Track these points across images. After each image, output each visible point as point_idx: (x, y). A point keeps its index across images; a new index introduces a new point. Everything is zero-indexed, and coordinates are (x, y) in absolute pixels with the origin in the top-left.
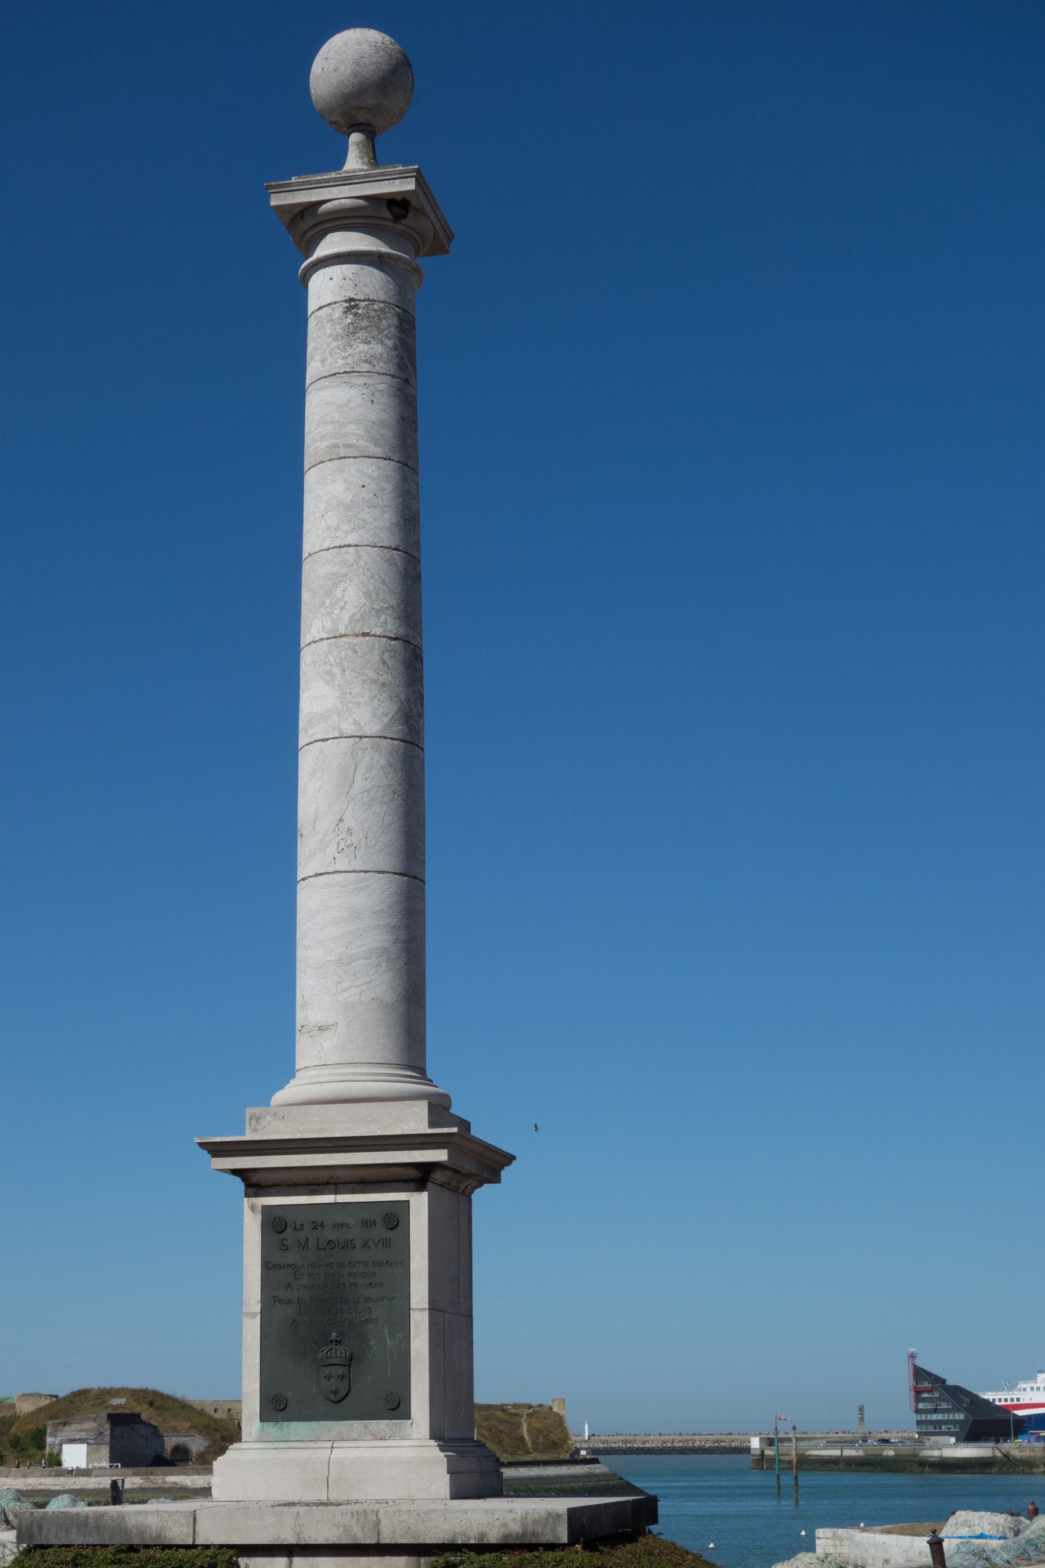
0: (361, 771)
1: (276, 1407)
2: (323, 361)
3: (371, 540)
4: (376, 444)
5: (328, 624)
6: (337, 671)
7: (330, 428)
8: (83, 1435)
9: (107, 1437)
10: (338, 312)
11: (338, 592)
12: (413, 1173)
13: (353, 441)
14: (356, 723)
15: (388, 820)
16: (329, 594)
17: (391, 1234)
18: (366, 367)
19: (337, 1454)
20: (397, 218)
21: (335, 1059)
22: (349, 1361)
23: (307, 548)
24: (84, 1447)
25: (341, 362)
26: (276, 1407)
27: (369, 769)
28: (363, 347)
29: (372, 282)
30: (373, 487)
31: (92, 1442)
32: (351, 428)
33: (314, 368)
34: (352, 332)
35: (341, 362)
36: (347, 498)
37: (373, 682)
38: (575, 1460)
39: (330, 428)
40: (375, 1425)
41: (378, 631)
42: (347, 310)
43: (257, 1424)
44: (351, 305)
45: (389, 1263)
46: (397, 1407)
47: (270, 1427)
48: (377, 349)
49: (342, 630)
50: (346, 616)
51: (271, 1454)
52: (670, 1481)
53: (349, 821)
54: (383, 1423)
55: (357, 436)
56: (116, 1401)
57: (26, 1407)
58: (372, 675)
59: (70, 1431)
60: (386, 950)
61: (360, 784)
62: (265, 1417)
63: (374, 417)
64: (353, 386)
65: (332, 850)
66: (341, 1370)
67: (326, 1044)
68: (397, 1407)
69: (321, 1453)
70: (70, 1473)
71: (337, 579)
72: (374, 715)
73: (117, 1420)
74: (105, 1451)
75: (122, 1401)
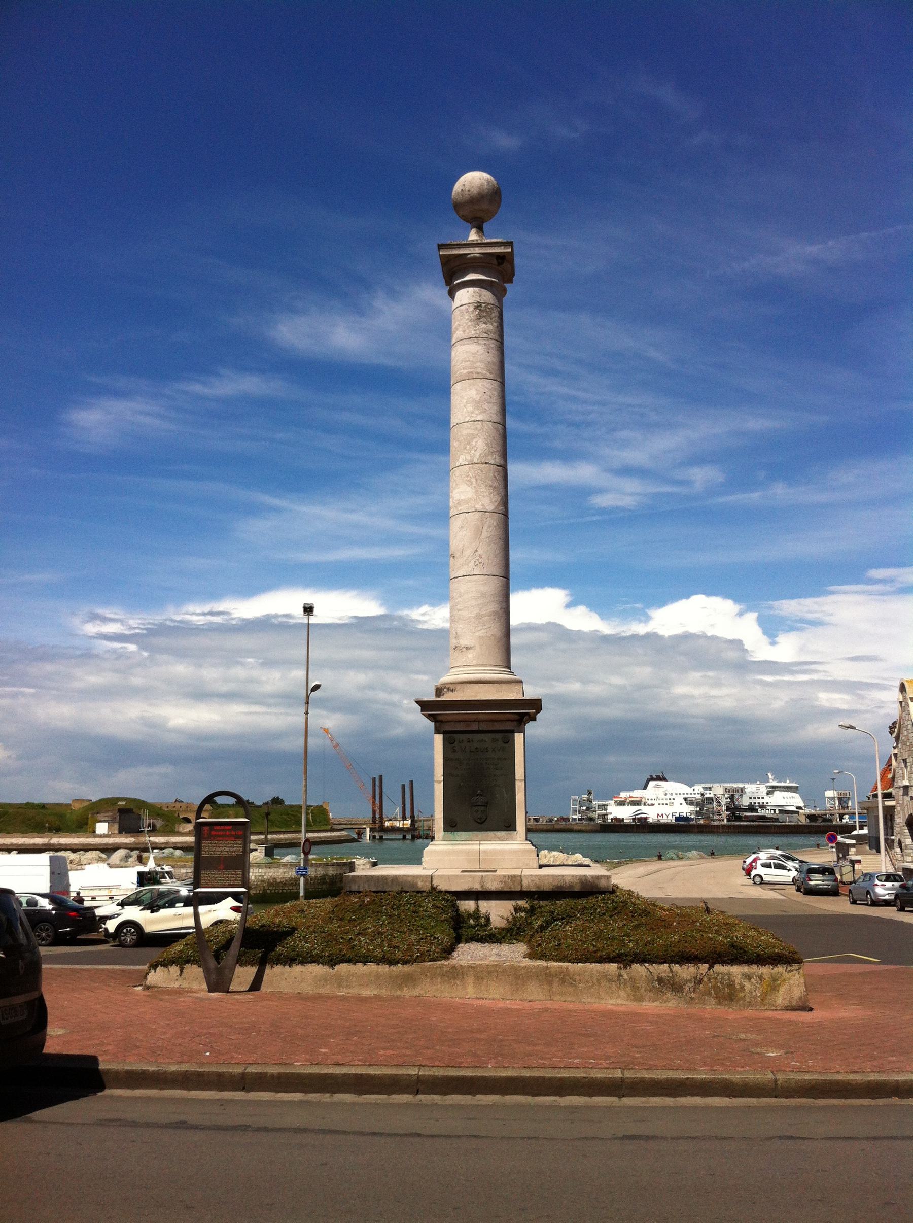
0: (485, 528)
1: (451, 825)
2: (464, 331)
3: (489, 419)
4: (491, 373)
5: (469, 458)
6: (473, 480)
7: (468, 364)
8: (106, 819)
9: (118, 819)
10: (471, 309)
11: (474, 443)
12: (517, 717)
13: (479, 371)
14: (483, 505)
15: (497, 551)
16: (469, 443)
17: (506, 745)
18: (485, 335)
19: (483, 847)
20: (499, 264)
21: (475, 662)
22: (486, 805)
23: (454, 420)
24: (106, 824)
25: (473, 332)
26: (451, 825)
27: (489, 527)
28: (484, 326)
29: (487, 296)
30: (489, 393)
31: (111, 822)
32: (479, 364)
33: (457, 335)
34: (479, 318)
35: (473, 332)
36: (477, 398)
37: (491, 486)
38: (332, 830)
39: (468, 364)
40: (499, 834)
41: (492, 462)
42: (476, 308)
43: (442, 833)
44: (478, 306)
45: (505, 759)
46: (510, 826)
47: (449, 834)
48: (490, 327)
49: (476, 461)
50: (478, 454)
51: (451, 847)
52: (280, 833)
53: (480, 551)
54: (503, 833)
55: (481, 367)
56: (120, 803)
57: (77, 806)
58: (490, 482)
59: (99, 817)
60: (497, 612)
61: (485, 534)
62: (446, 830)
63: (489, 359)
64: (479, 344)
65: (472, 564)
66: (483, 808)
67: (470, 656)
68: (510, 826)
69: (474, 847)
70: (101, 836)
71: (473, 437)
72: (491, 502)
73: (122, 811)
74: (116, 826)
75: (124, 803)
